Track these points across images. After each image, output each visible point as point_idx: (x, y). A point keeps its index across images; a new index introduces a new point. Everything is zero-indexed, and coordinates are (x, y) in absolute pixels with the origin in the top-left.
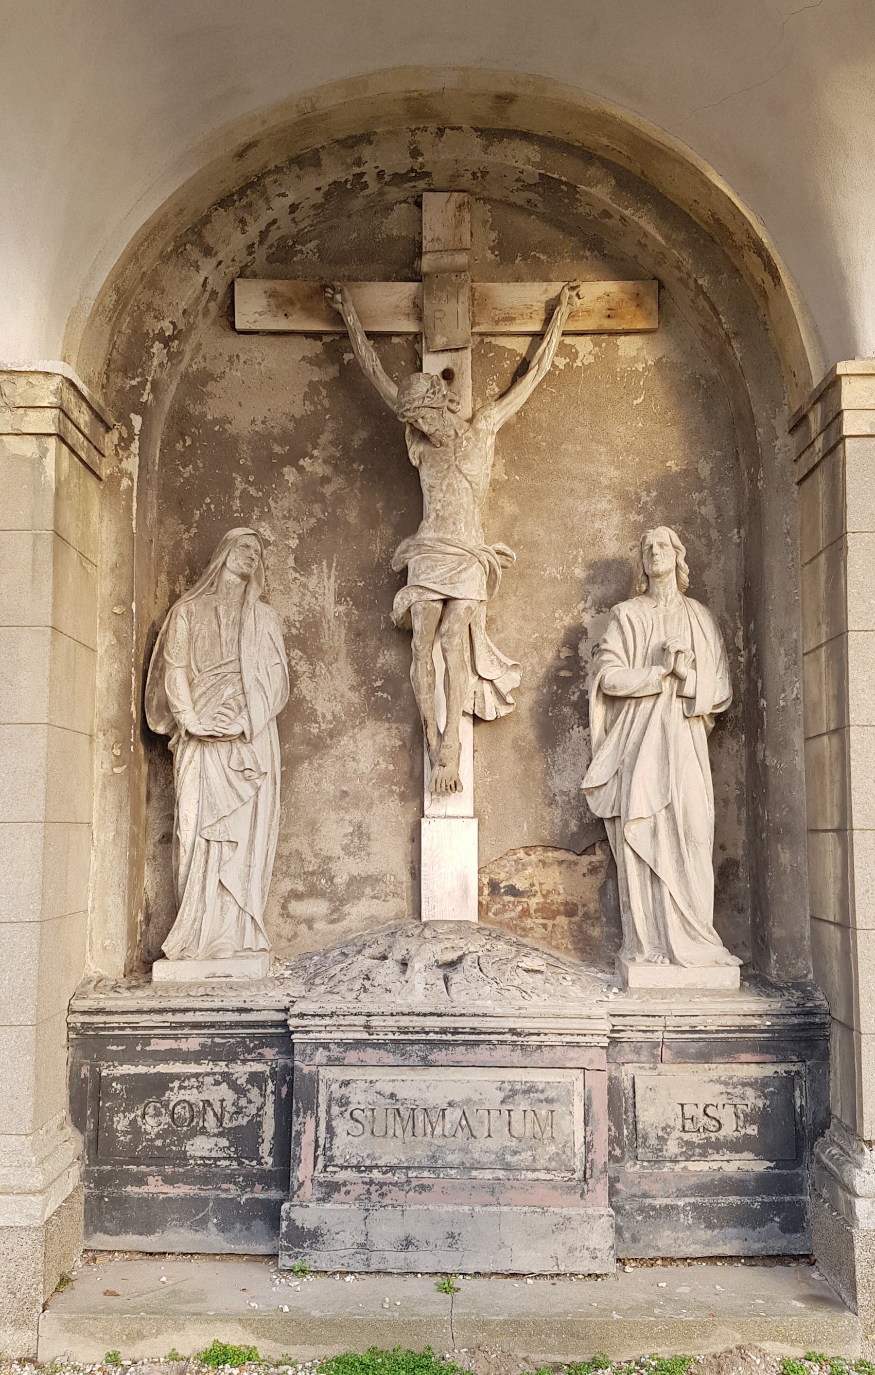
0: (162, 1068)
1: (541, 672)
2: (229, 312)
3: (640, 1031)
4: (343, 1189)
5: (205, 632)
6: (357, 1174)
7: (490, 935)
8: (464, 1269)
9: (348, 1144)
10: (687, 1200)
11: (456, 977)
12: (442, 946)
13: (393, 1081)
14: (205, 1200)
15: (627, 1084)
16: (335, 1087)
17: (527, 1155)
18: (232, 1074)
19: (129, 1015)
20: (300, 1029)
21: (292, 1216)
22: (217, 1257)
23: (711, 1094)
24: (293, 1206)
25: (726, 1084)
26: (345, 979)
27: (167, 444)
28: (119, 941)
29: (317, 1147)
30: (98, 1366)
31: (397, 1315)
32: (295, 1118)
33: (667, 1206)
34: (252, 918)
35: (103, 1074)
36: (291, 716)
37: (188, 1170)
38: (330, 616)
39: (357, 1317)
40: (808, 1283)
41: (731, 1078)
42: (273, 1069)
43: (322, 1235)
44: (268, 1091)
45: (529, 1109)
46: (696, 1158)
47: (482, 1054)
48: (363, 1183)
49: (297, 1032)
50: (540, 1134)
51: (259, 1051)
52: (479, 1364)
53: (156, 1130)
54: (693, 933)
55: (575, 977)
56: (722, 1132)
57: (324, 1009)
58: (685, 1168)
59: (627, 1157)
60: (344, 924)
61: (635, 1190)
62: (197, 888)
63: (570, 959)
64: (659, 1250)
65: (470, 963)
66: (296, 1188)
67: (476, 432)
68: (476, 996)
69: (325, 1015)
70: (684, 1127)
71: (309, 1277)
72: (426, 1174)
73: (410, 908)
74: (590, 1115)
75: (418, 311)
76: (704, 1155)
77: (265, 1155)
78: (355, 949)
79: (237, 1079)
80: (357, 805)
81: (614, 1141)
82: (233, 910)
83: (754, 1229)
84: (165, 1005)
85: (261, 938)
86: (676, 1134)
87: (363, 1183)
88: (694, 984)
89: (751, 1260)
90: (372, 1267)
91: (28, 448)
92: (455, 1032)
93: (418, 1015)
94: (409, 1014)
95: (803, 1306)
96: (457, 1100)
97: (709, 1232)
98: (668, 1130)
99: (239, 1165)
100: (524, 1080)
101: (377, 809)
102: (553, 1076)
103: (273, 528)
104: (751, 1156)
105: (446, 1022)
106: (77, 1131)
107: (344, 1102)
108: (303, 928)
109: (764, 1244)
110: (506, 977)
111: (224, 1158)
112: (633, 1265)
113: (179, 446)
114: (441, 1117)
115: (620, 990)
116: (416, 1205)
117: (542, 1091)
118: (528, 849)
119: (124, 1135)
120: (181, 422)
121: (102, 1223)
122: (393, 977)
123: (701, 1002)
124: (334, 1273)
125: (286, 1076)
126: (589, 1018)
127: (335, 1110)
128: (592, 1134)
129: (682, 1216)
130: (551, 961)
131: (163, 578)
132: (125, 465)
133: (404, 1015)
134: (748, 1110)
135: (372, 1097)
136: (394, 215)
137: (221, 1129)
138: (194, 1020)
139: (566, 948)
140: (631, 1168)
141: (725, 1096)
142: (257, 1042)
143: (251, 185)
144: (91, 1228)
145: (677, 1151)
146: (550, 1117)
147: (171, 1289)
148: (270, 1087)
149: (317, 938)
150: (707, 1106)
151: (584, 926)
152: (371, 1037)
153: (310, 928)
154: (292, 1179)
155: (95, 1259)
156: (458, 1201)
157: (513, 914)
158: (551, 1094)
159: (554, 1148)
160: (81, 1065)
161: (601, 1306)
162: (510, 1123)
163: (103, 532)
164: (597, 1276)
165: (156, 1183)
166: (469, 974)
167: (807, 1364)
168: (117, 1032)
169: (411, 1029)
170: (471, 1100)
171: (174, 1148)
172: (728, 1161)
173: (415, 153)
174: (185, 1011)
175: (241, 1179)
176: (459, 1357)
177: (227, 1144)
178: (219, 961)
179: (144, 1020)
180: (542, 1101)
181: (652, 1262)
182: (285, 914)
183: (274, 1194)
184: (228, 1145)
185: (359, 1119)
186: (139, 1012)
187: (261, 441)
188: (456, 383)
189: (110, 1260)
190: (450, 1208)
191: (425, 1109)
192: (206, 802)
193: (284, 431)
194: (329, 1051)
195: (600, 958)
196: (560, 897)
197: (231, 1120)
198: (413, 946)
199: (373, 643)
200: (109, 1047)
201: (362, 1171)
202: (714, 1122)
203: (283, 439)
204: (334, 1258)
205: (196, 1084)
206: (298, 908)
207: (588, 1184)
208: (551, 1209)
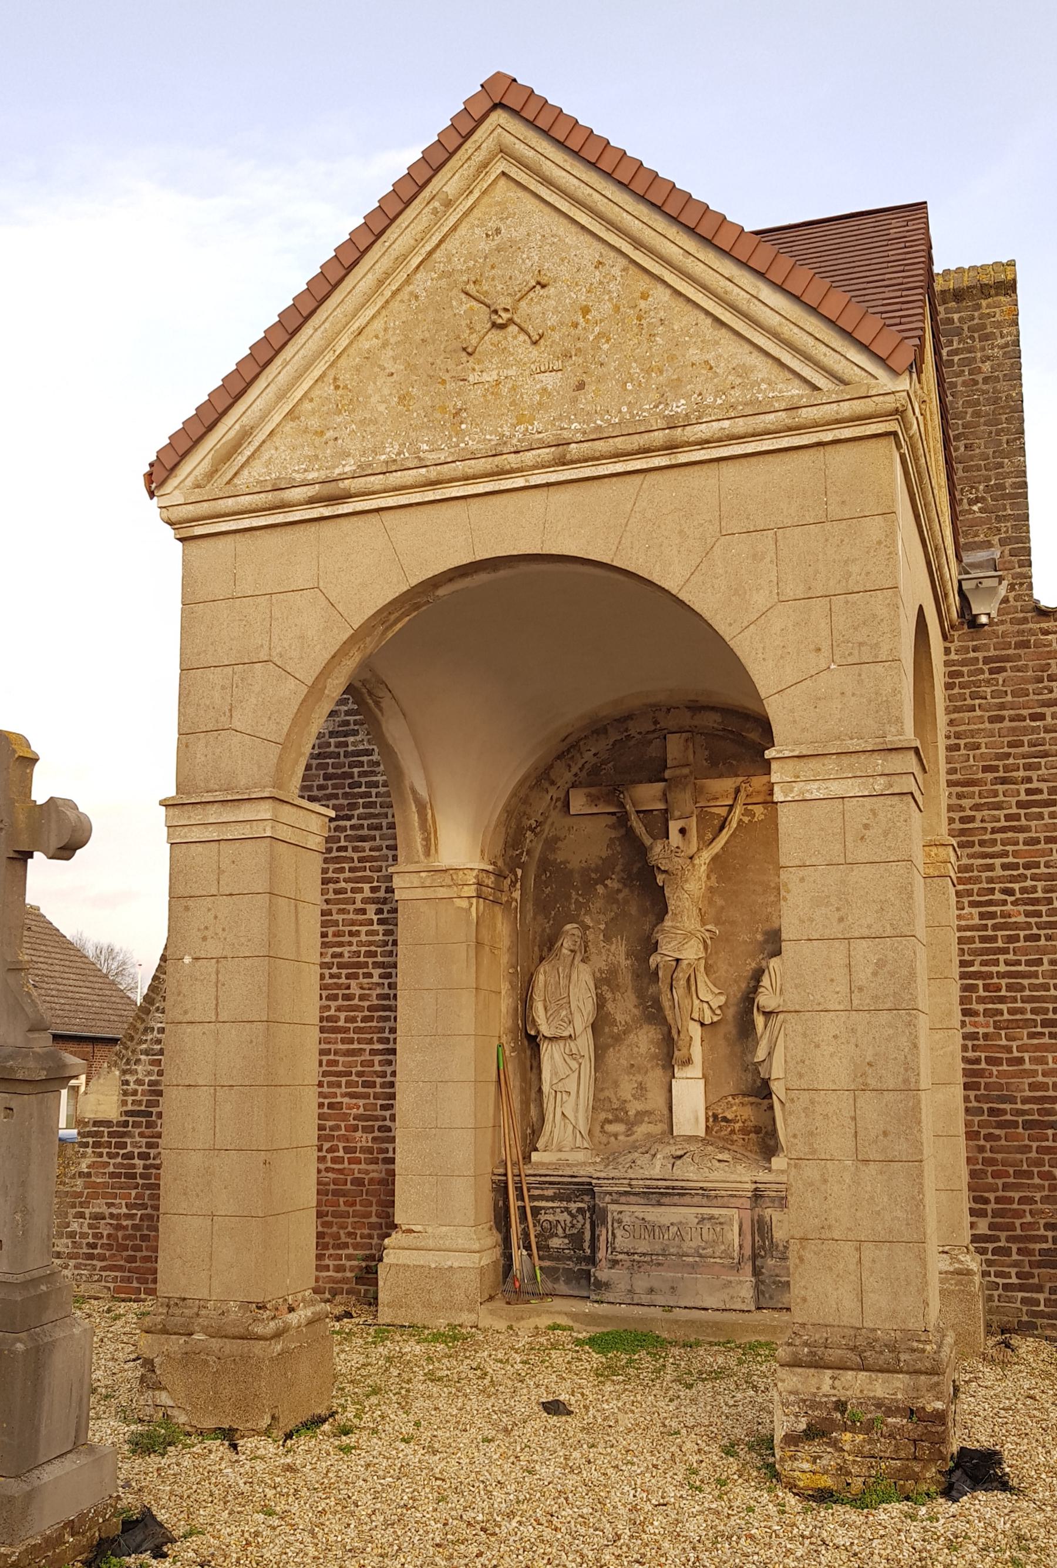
1: (739, 995)
2: (567, 805)
15: (768, 1219)
16: (615, 1214)
17: (710, 1250)
27: (537, 877)
47: (687, 1200)
60: (634, 1137)
62: (552, 1115)
67: (694, 866)
75: (665, 798)
80: (639, 1072)
82: (570, 1127)
84: (536, 1172)
92: (673, 1188)
101: (650, 1074)
107: (620, 1222)
108: (613, 1139)
113: (543, 877)
118: (733, 1096)
120: (544, 864)
125: (593, 1209)
127: (616, 1225)
131: (536, 949)
132: (514, 895)
143: (572, 747)
148: (588, 1215)
158: (722, 1220)
163: (502, 928)
173: (656, 723)
174: (546, 1176)
182: (603, 1131)
188: (687, 834)
192: (555, 1073)
199: (646, 980)
203: (596, 870)
206: (610, 1128)
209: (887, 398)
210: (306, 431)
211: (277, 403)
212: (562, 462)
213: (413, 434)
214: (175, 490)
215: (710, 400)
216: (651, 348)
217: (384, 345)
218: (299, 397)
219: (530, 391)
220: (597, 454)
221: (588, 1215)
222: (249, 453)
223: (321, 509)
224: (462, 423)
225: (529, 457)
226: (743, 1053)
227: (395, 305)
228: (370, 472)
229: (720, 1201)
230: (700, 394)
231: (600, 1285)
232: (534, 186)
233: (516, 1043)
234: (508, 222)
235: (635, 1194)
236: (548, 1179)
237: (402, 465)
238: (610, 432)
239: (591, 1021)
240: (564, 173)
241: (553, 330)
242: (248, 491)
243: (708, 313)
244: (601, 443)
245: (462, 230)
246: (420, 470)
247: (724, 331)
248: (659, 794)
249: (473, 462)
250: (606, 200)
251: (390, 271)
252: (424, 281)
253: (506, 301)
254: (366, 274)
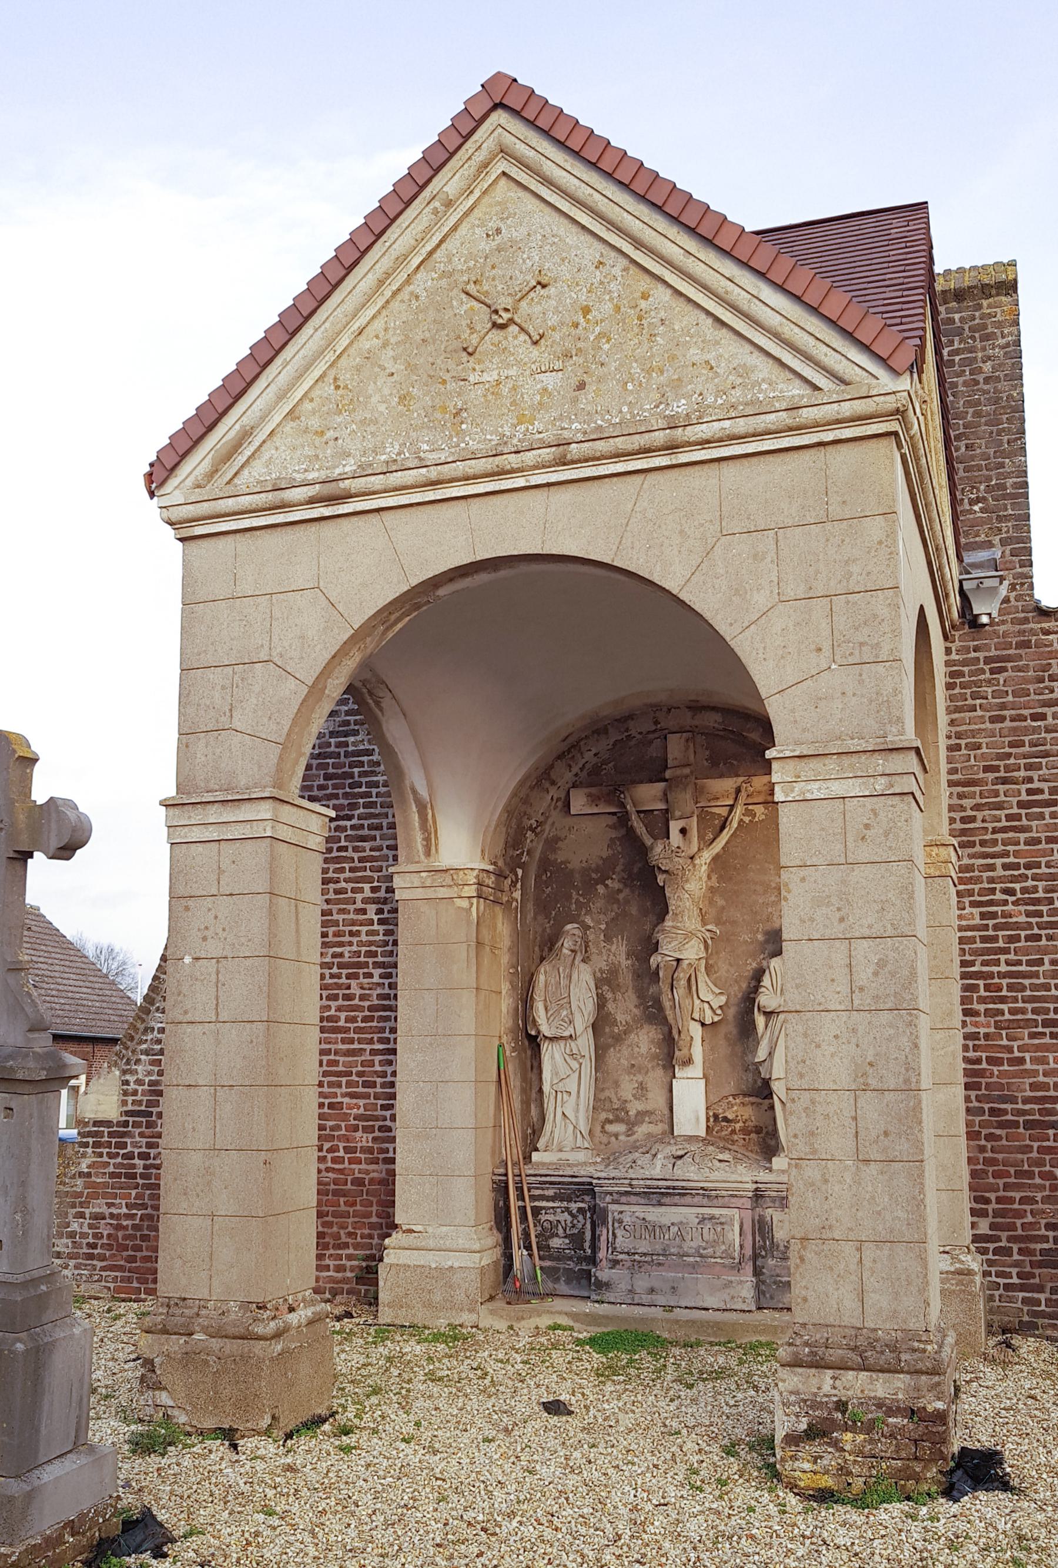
1: (740, 995)
2: (567, 805)
5: (553, 981)
15: (769, 1219)
16: (616, 1214)
17: (710, 1250)
27: (538, 877)
36: (600, 1023)
38: (623, 967)
47: (688, 1200)
60: (635, 1137)
61: (773, 1273)
62: (552, 1115)
75: (665, 798)
80: (640, 1072)
82: (571, 1128)
84: (536, 1172)
91: (465, 903)
92: (674, 1188)
103: (592, 919)
105: (669, 1183)
107: (620, 1222)
108: (613, 1139)
113: (544, 877)
118: (734, 1096)
120: (545, 864)
125: (593, 1209)
131: (537, 949)
135: (634, 1219)
136: (654, 745)
148: (588, 1215)
158: (723, 1220)
163: (503, 929)
173: (656, 723)
174: (546, 1176)
182: (603, 1131)
187: (585, 872)
188: (688, 835)
192: (555, 1073)
193: (598, 866)
199: (647, 980)
203: (596, 871)
206: (610, 1128)
209: (888, 398)
210: (306, 431)
211: (277, 403)
212: (563, 462)
213: (414, 435)
214: (175, 490)
215: (710, 400)
216: (651, 348)
217: (385, 345)
218: (299, 397)
219: (530, 392)
220: (598, 454)
221: (588, 1215)
222: (249, 454)
223: (321, 509)
224: (462, 423)
225: (529, 458)
226: (744, 1053)
227: (395, 305)
228: (370, 472)
229: (721, 1202)
230: (701, 394)
231: (601, 1285)
232: (534, 186)
233: (516, 1043)
234: (508, 222)
235: (635, 1194)
236: (548, 1179)
237: (403, 465)
238: (610, 432)
239: (592, 1021)
240: (564, 173)
241: (553, 330)
242: (248, 491)
243: (708, 313)
244: (601, 443)
245: (463, 230)
246: (420, 470)
247: (724, 331)
248: (660, 794)
249: (473, 461)
250: (607, 200)
251: (390, 271)
252: (424, 281)
253: (506, 301)
254: (367, 274)
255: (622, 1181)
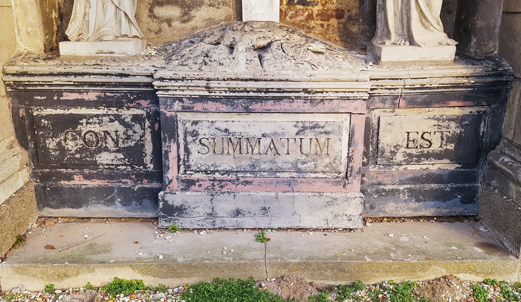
0: (73, 111)
3: (386, 89)
4: (197, 184)
6: (205, 175)
7: (288, 30)
8: (272, 226)
9: (198, 157)
10: (406, 186)
11: (267, 56)
12: (257, 36)
13: (227, 121)
14: (112, 189)
15: (375, 121)
16: (188, 125)
18: (121, 116)
19: (45, 77)
20: (162, 88)
21: (166, 199)
22: (123, 220)
23: (428, 126)
24: (165, 193)
25: (438, 120)
26: (192, 56)
28: (37, 29)
29: (179, 160)
30: (40, 294)
31: (231, 259)
32: (163, 143)
33: (393, 190)
34: (126, 14)
35: (34, 114)
37: (99, 172)
39: (206, 262)
40: (478, 234)
41: (442, 116)
42: (147, 113)
43: (185, 209)
44: (146, 126)
45: (313, 137)
46: (413, 163)
47: (285, 105)
48: (209, 180)
49: (160, 90)
50: (320, 152)
51: (137, 102)
52: (283, 290)
53: (75, 148)
54: (426, 24)
55: (343, 56)
56: (432, 148)
57: (178, 75)
58: (406, 168)
59: (370, 162)
61: (374, 181)
63: (337, 46)
64: (386, 213)
65: (276, 47)
66: (167, 183)
68: (281, 68)
69: (178, 79)
70: (408, 145)
71: (178, 232)
72: (248, 175)
73: (235, 13)
74: (353, 141)
76: (418, 161)
77: (148, 163)
78: (199, 39)
79: (124, 119)
81: (365, 154)
83: (445, 202)
84: (68, 70)
85: (133, 29)
86: (403, 149)
87: (209, 180)
88: (425, 58)
89: (440, 219)
90: (216, 226)
92: (267, 91)
93: (242, 80)
94: (236, 80)
95: (482, 251)
96: (268, 133)
97: (417, 204)
98: (398, 147)
99: (131, 168)
100: (311, 120)
102: (330, 118)
104: (448, 161)
106: (23, 149)
107: (195, 134)
108: (165, 25)
109: (449, 210)
110: (301, 56)
111: (122, 165)
112: (370, 221)
114: (257, 143)
115: (374, 63)
116: (243, 192)
117: (323, 127)
119: (54, 152)
121: (48, 202)
122: (224, 56)
123: (430, 70)
124: (194, 229)
125: (155, 117)
126: (357, 81)
127: (190, 139)
128: (353, 151)
129: (401, 195)
130: (328, 47)
133: (232, 80)
134: (450, 135)
135: (213, 131)
137: (118, 148)
138: (89, 81)
139: (335, 39)
140: (372, 169)
141: (436, 127)
142: (135, 96)
144: (41, 205)
145: (402, 159)
146: (327, 142)
147: (89, 243)
148: (147, 123)
149: (175, 32)
150: (424, 133)
151: (348, 25)
152: (211, 94)
153: (170, 25)
154: (164, 178)
155: (44, 223)
156: (268, 190)
157: (302, 18)
158: (328, 128)
159: (328, 160)
160: (19, 108)
161: (357, 252)
162: (301, 146)
164: (351, 230)
165: (79, 179)
166: (276, 54)
167: (486, 286)
168: (39, 88)
169: (237, 89)
170: (277, 133)
171: (88, 159)
172: (433, 164)
174: (83, 74)
175: (134, 176)
176: (270, 286)
177: (122, 157)
178: (104, 42)
179: (55, 80)
180: (322, 133)
181: (381, 220)
182: (152, 15)
183: (155, 185)
184: (123, 157)
185: (205, 144)
186: (51, 74)
189: (55, 223)
190: (264, 194)
191: (248, 138)
194: (183, 102)
195: (356, 45)
196: (334, 6)
197: (123, 142)
198: (237, 36)
200: (36, 97)
201: (209, 174)
202: (427, 142)
204: (193, 221)
205: (98, 121)
207: (348, 180)
208: (325, 194)
221: (147, 123)
229: (327, 106)
231: (171, 211)
235: (215, 100)
236: (86, 79)
255: (195, 83)
